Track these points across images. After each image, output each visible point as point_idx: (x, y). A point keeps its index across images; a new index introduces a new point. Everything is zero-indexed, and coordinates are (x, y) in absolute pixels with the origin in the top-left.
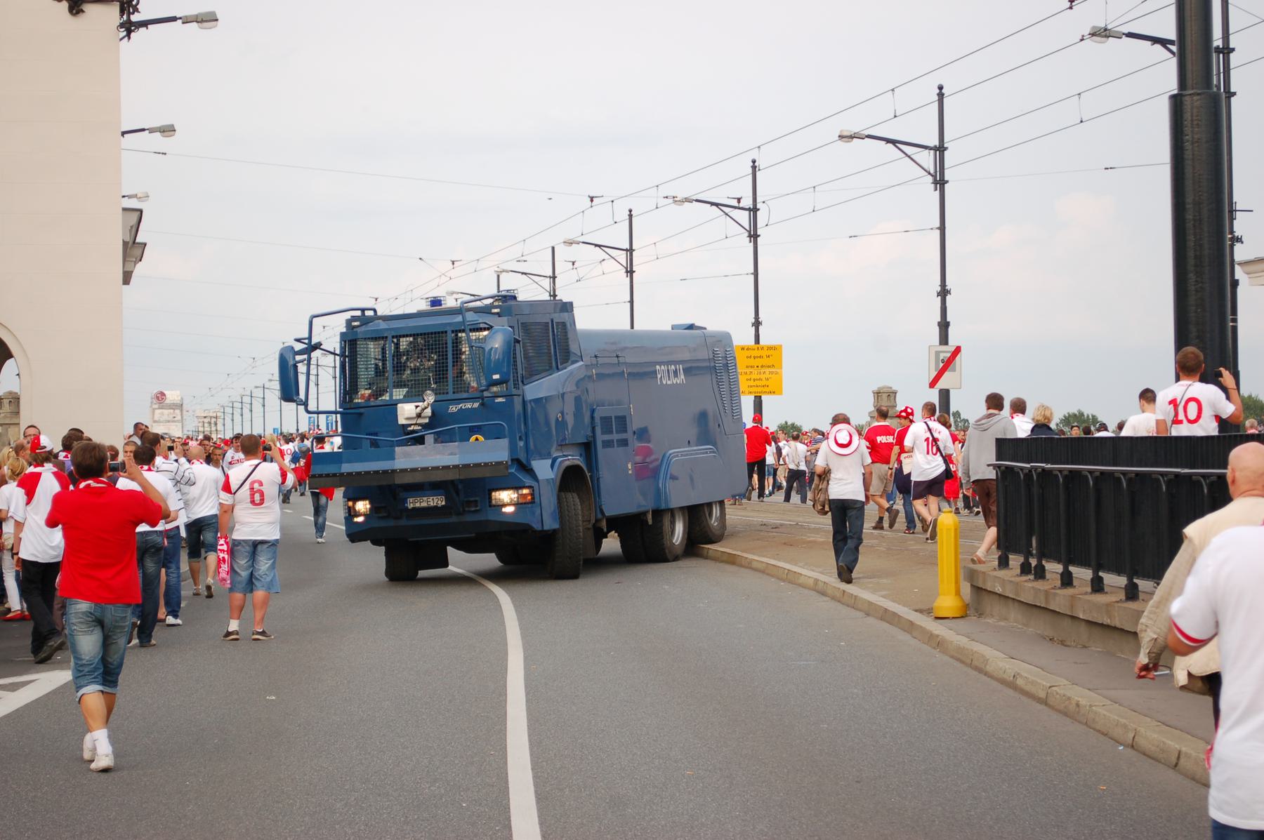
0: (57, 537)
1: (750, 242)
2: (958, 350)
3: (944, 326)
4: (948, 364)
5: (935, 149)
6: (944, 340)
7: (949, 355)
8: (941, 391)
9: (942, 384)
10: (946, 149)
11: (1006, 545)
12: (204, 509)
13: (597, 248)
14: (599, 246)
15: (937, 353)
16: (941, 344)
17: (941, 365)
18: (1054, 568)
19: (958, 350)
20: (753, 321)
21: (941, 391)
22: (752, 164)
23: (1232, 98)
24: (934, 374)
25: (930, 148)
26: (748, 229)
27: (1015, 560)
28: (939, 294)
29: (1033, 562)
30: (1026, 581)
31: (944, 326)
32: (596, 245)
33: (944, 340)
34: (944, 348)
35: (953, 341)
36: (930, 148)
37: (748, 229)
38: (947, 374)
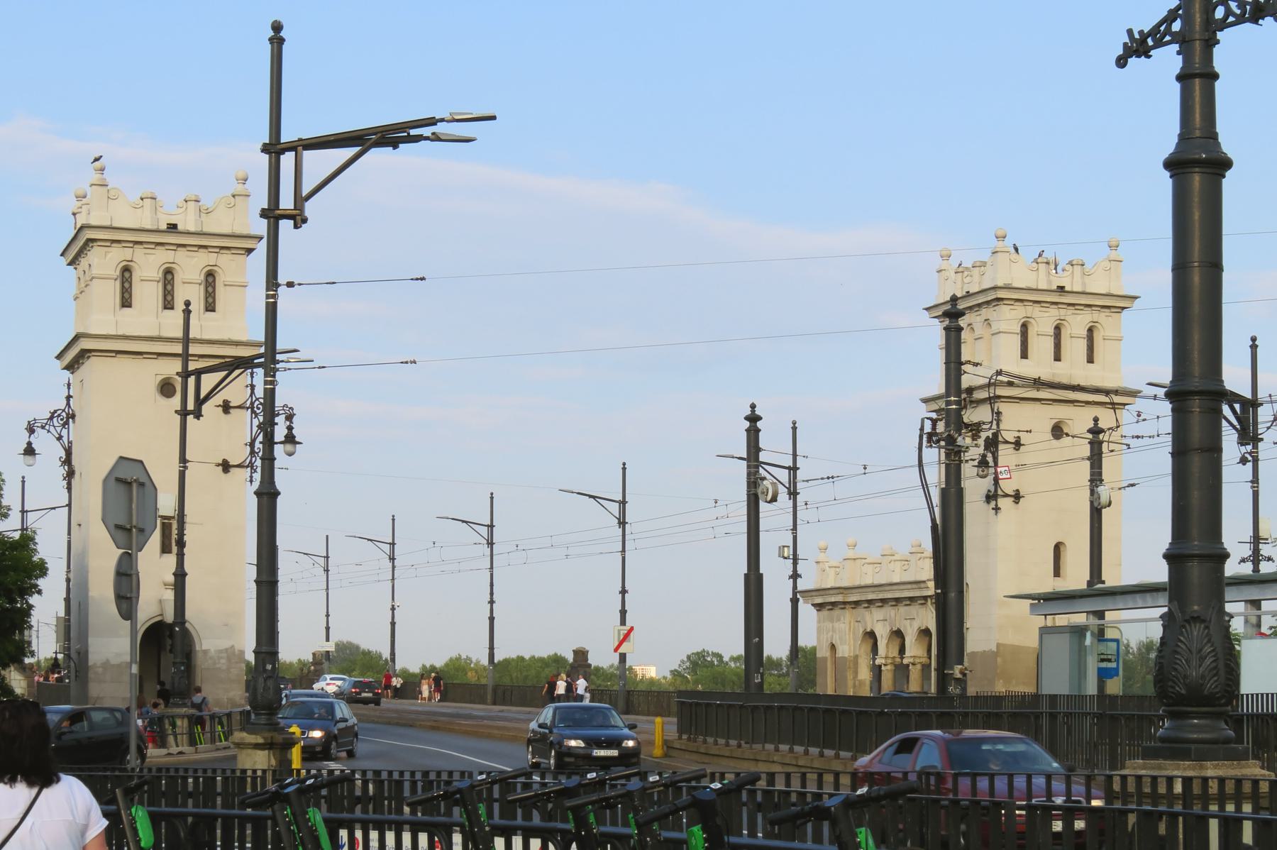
0: (1229, 608)
1: (790, 499)
2: (632, 629)
3: (623, 613)
4: (627, 636)
5: (619, 502)
6: (623, 622)
7: (626, 632)
8: (620, 654)
9: (621, 650)
10: (627, 502)
11: (681, 731)
12: (849, 637)
13: (370, 542)
14: (466, 522)
15: (619, 631)
16: (621, 625)
17: (622, 638)
18: (701, 738)
19: (632, 629)
20: (621, 589)
21: (620, 654)
22: (622, 466)
23: (1259, 408)
24: (617, 644)
25: (486, 526)
26: (787, 486)
27: (685, 737)
28: (620, 593)
29: (692, 736)
30: (1181, 683)
31: (623, 613)
32: (463, 521)
33: (623, 622)
34: (623, 627)
35: (629, 624)
36: (486, 526)
37: (787, 486)
38: (625, 644)
